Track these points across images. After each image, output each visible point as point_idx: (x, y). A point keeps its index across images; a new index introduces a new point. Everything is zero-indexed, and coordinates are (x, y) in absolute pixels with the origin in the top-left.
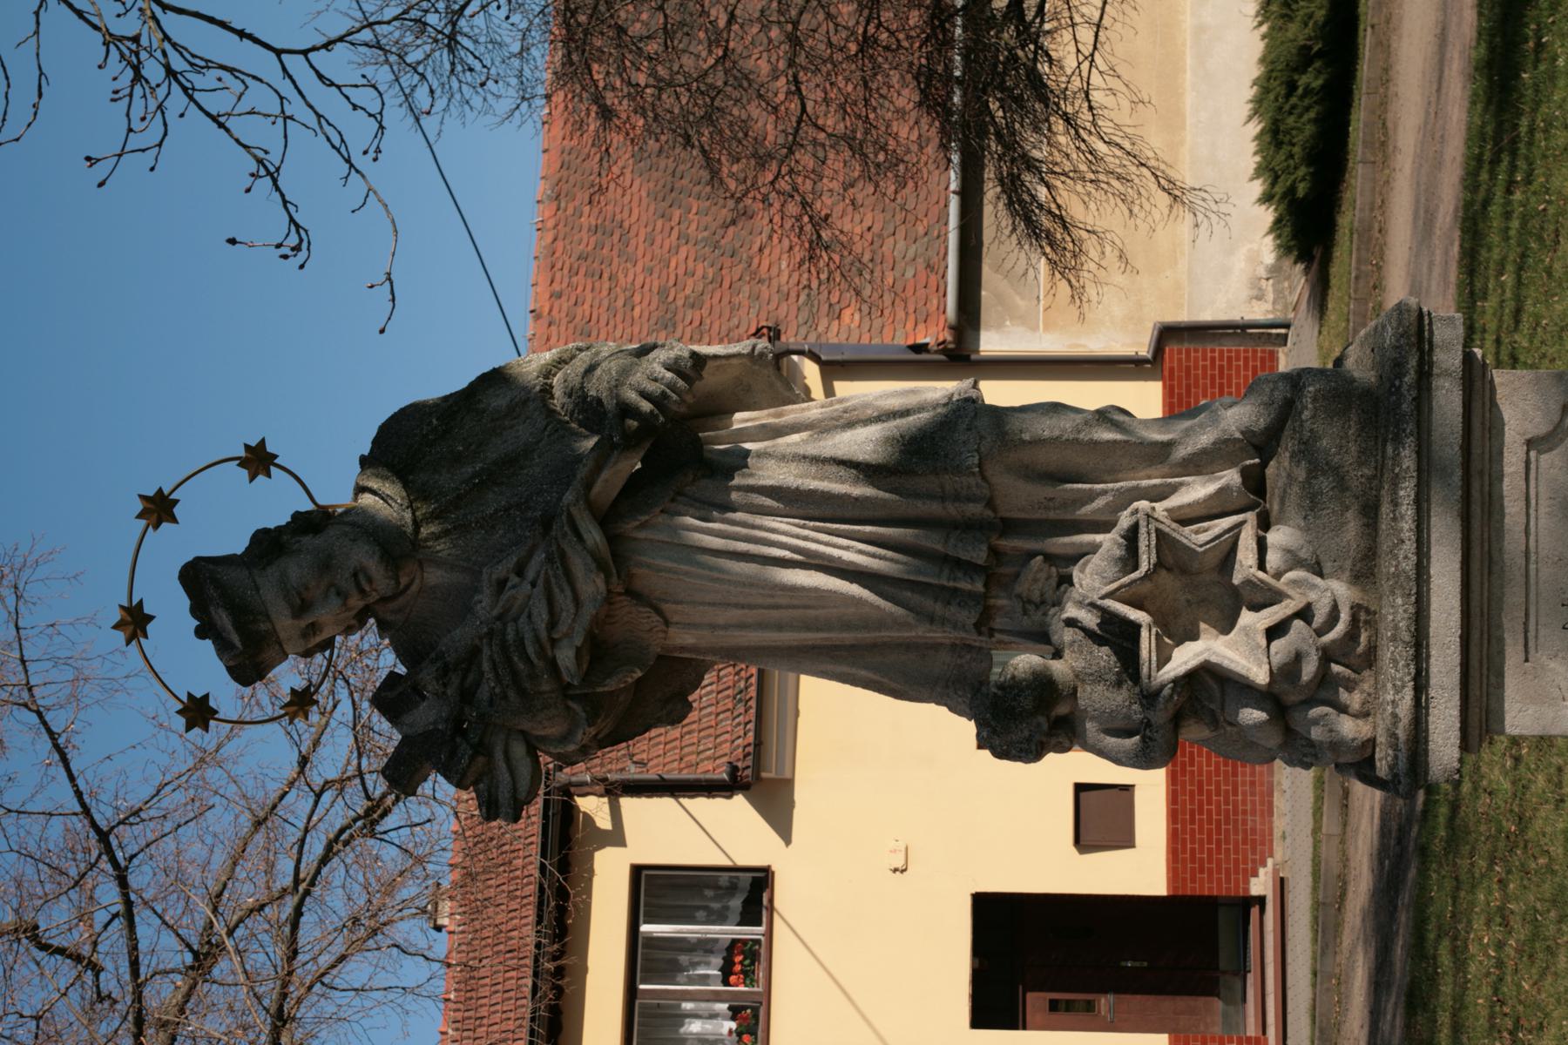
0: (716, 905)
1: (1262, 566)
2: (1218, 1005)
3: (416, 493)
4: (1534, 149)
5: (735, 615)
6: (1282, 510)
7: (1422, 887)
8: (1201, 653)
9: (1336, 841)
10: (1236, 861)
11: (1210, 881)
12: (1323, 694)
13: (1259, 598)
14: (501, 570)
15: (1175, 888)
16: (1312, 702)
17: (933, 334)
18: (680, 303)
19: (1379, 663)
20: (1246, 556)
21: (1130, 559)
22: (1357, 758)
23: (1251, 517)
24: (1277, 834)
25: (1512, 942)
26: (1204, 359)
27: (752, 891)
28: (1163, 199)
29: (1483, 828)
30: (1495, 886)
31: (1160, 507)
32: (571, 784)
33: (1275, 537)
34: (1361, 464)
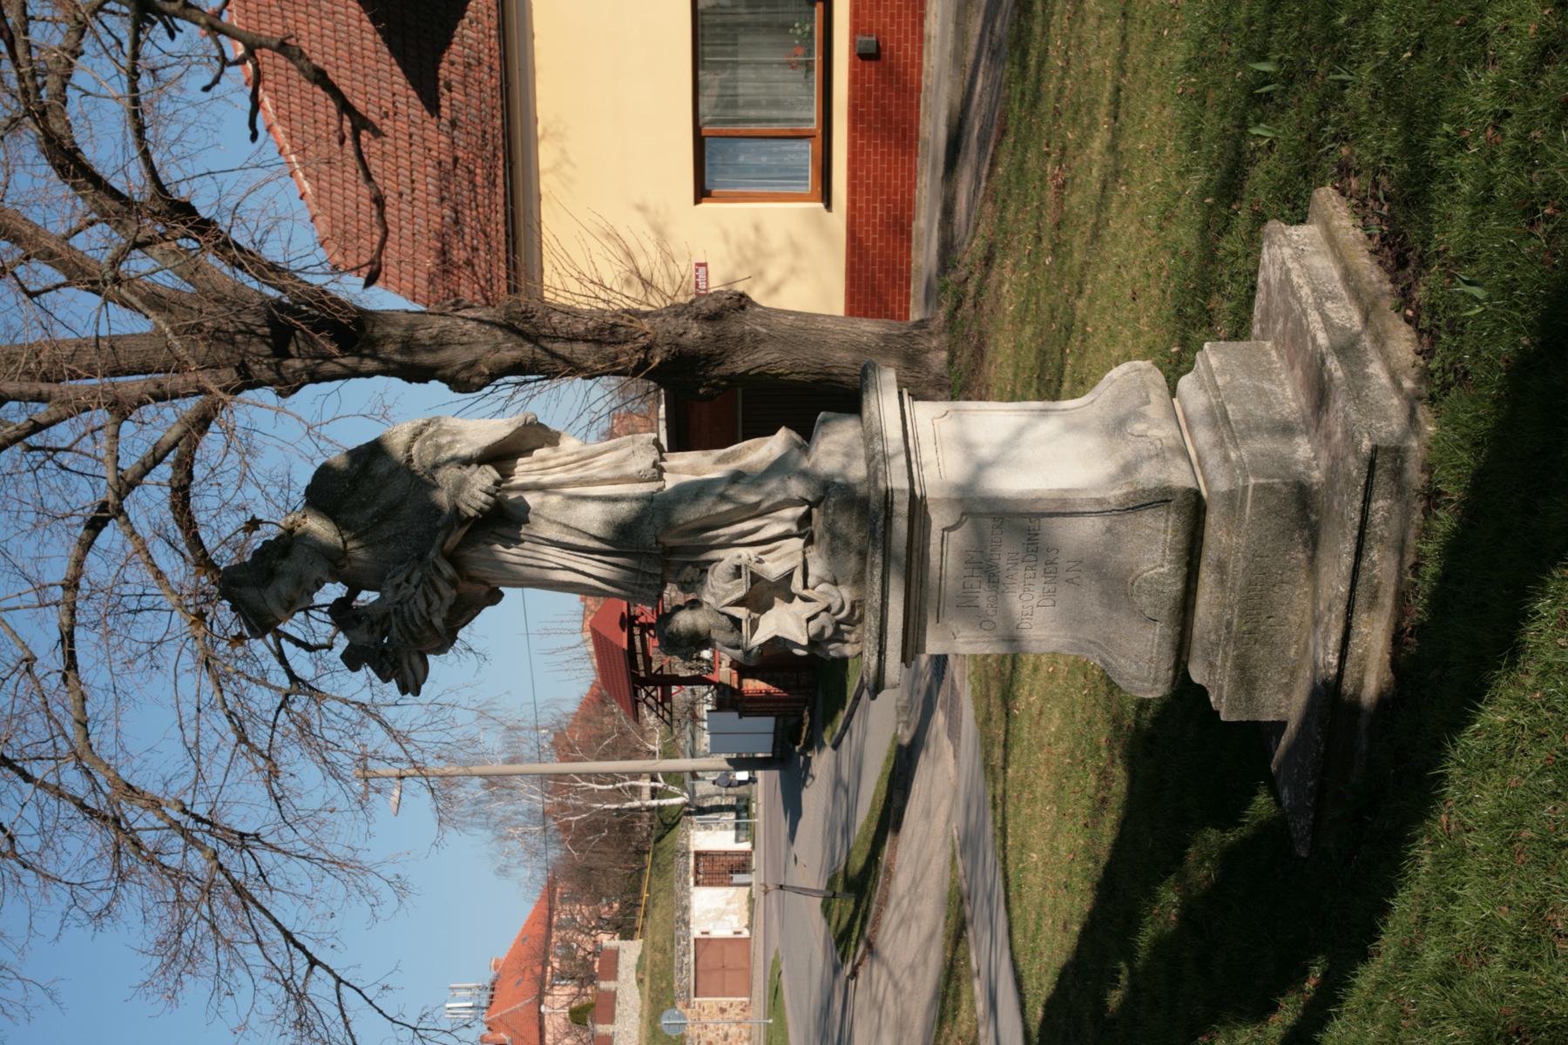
14: (397, 581)
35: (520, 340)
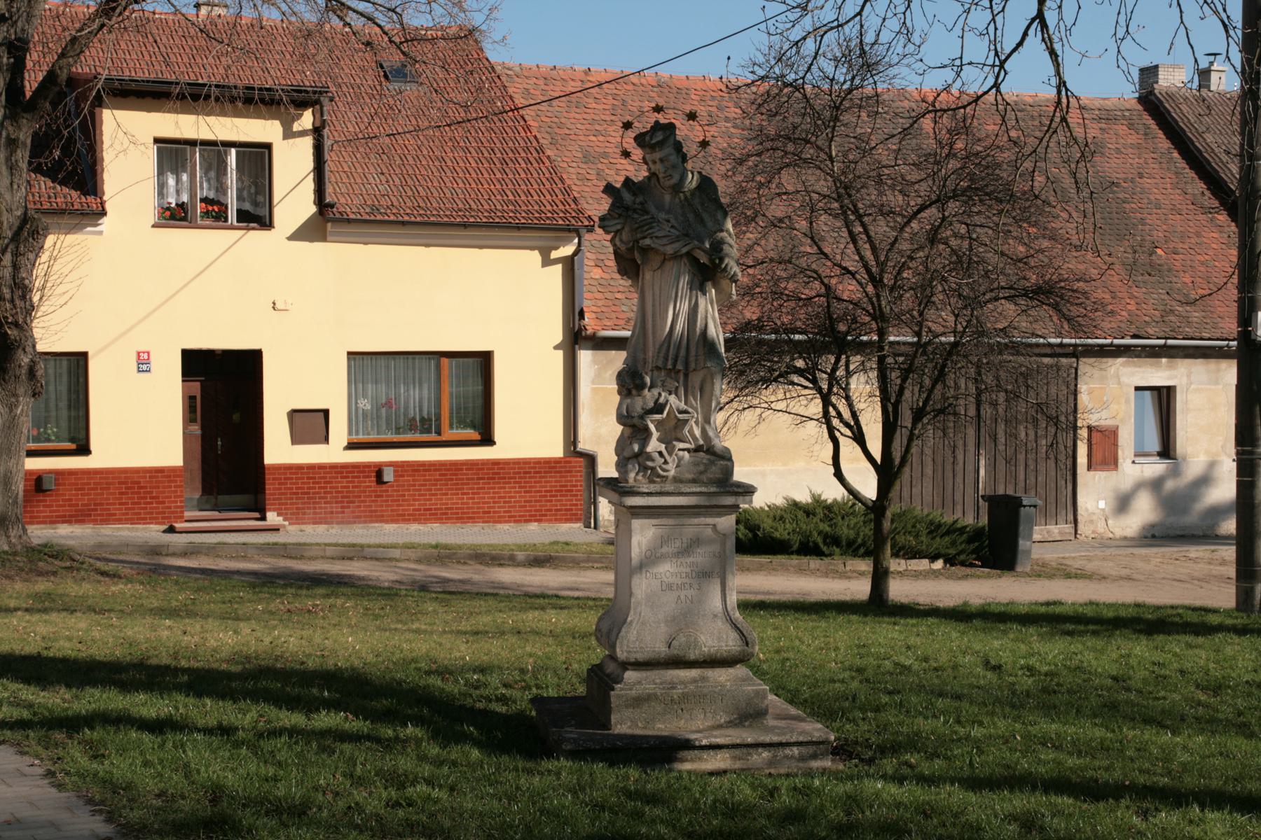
0: (245, 194)
2: (197, 495)
3: (693, 192)
5: (657, 292)
14: (673, 221)
17: (590, 322)
18: (600, 166)
20: (682, 445)
21: (681, 412)
24: (303, 527)
27: (257, 216)
32: (322, 107)
35: (15, 228)
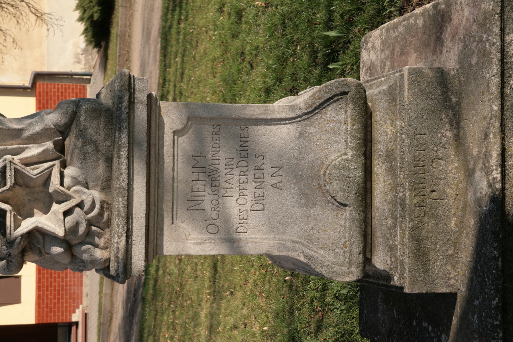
1: (62, 184)
4: (188, 6)
6: (71, 160)
7: (143, 315)
8: (34, 223)
9: (109, 296)
10: (66, 307)
11: (55, 316)
12: (88, 240)
13: (61, 198)
15: (39, 320)
16: (82, 243)
19: (112, 226)
20: (55, 180)
22: (103, 267)
23: (57, 163)
24: (84, 294)
25: (176, 336)
26: (54, 88)
28: (33, 17)
29: (167, 289)
30: (171, 313)
31: (16, 158)
33: (69, 171)
34: (105, 140)
